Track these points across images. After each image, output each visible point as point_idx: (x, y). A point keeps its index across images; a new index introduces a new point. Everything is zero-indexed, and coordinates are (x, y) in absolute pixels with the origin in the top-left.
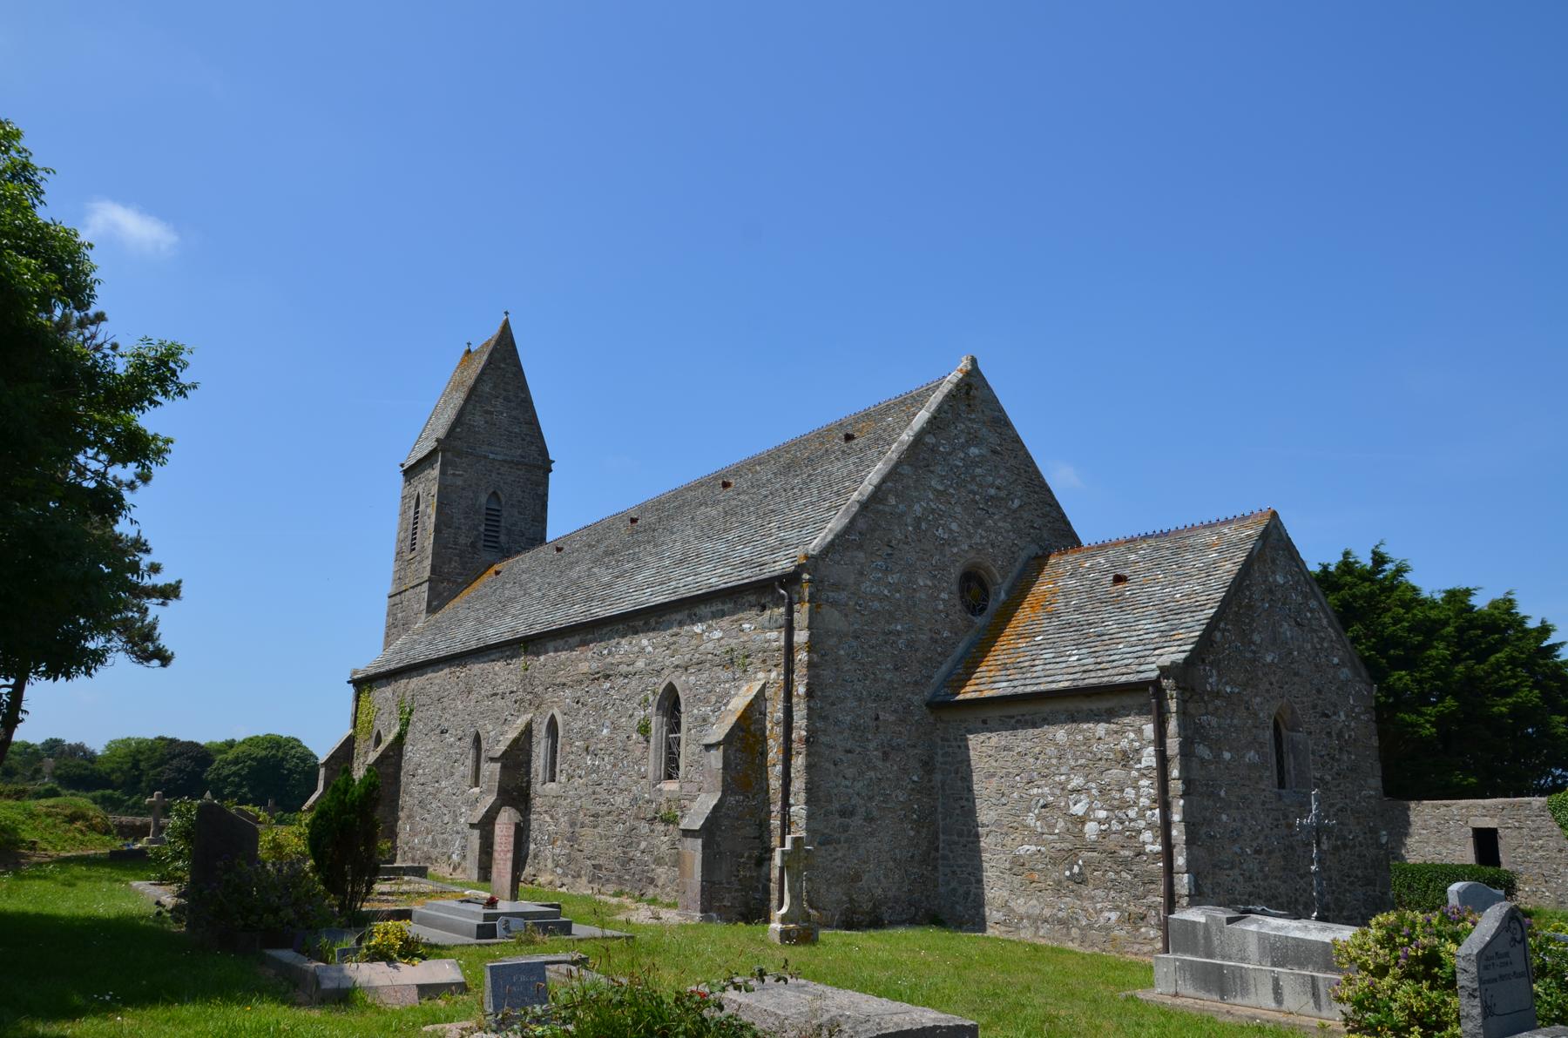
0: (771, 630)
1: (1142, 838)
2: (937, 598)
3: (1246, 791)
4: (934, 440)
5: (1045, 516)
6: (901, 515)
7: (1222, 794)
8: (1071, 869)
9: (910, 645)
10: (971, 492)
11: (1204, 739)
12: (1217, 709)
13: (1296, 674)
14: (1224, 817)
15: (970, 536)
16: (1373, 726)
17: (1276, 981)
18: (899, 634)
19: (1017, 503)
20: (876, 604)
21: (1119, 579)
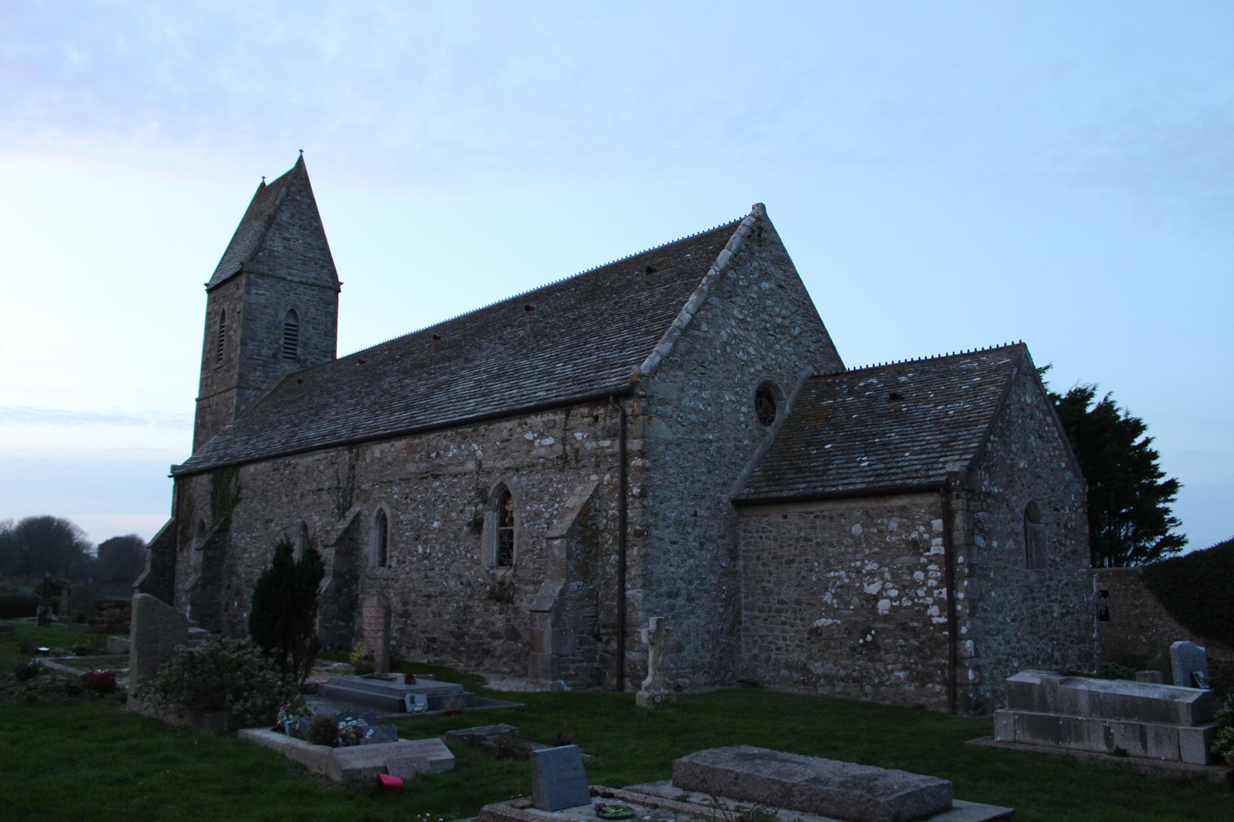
0: (604, 439)
1: (929, 612)
2: (739, 411)
3: (1007, 572)
4: (735, 276)
5: (818, 341)
6: (711, 341)
7: (992, 575)
8: (864, 638)
9: (719, 450)
10: (763, 320)
11: (981, 530)
12: (988, 507)
13: (1039, 477)
14: (993, 593)
15: (763, 359)
16: (1086, 517)
17: (1107, 730)
18: (710, 442)
19: (797, 331)
20: (693, 417)
21: (895, 397)
